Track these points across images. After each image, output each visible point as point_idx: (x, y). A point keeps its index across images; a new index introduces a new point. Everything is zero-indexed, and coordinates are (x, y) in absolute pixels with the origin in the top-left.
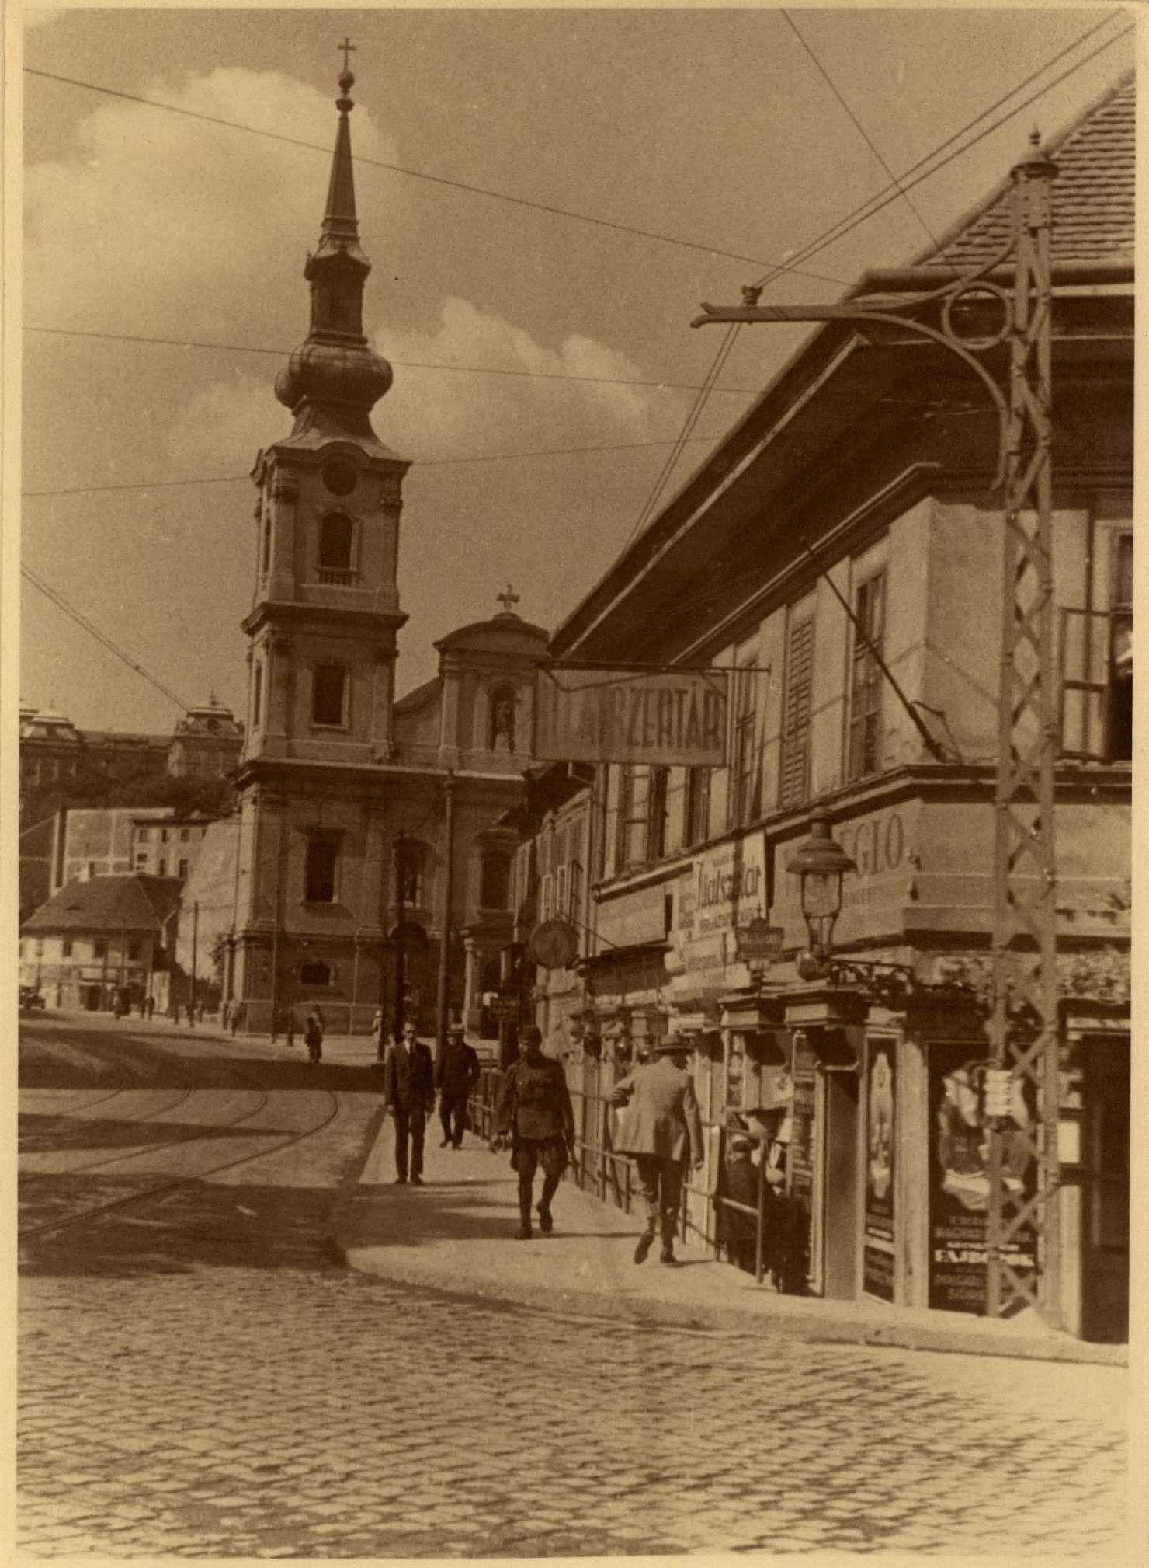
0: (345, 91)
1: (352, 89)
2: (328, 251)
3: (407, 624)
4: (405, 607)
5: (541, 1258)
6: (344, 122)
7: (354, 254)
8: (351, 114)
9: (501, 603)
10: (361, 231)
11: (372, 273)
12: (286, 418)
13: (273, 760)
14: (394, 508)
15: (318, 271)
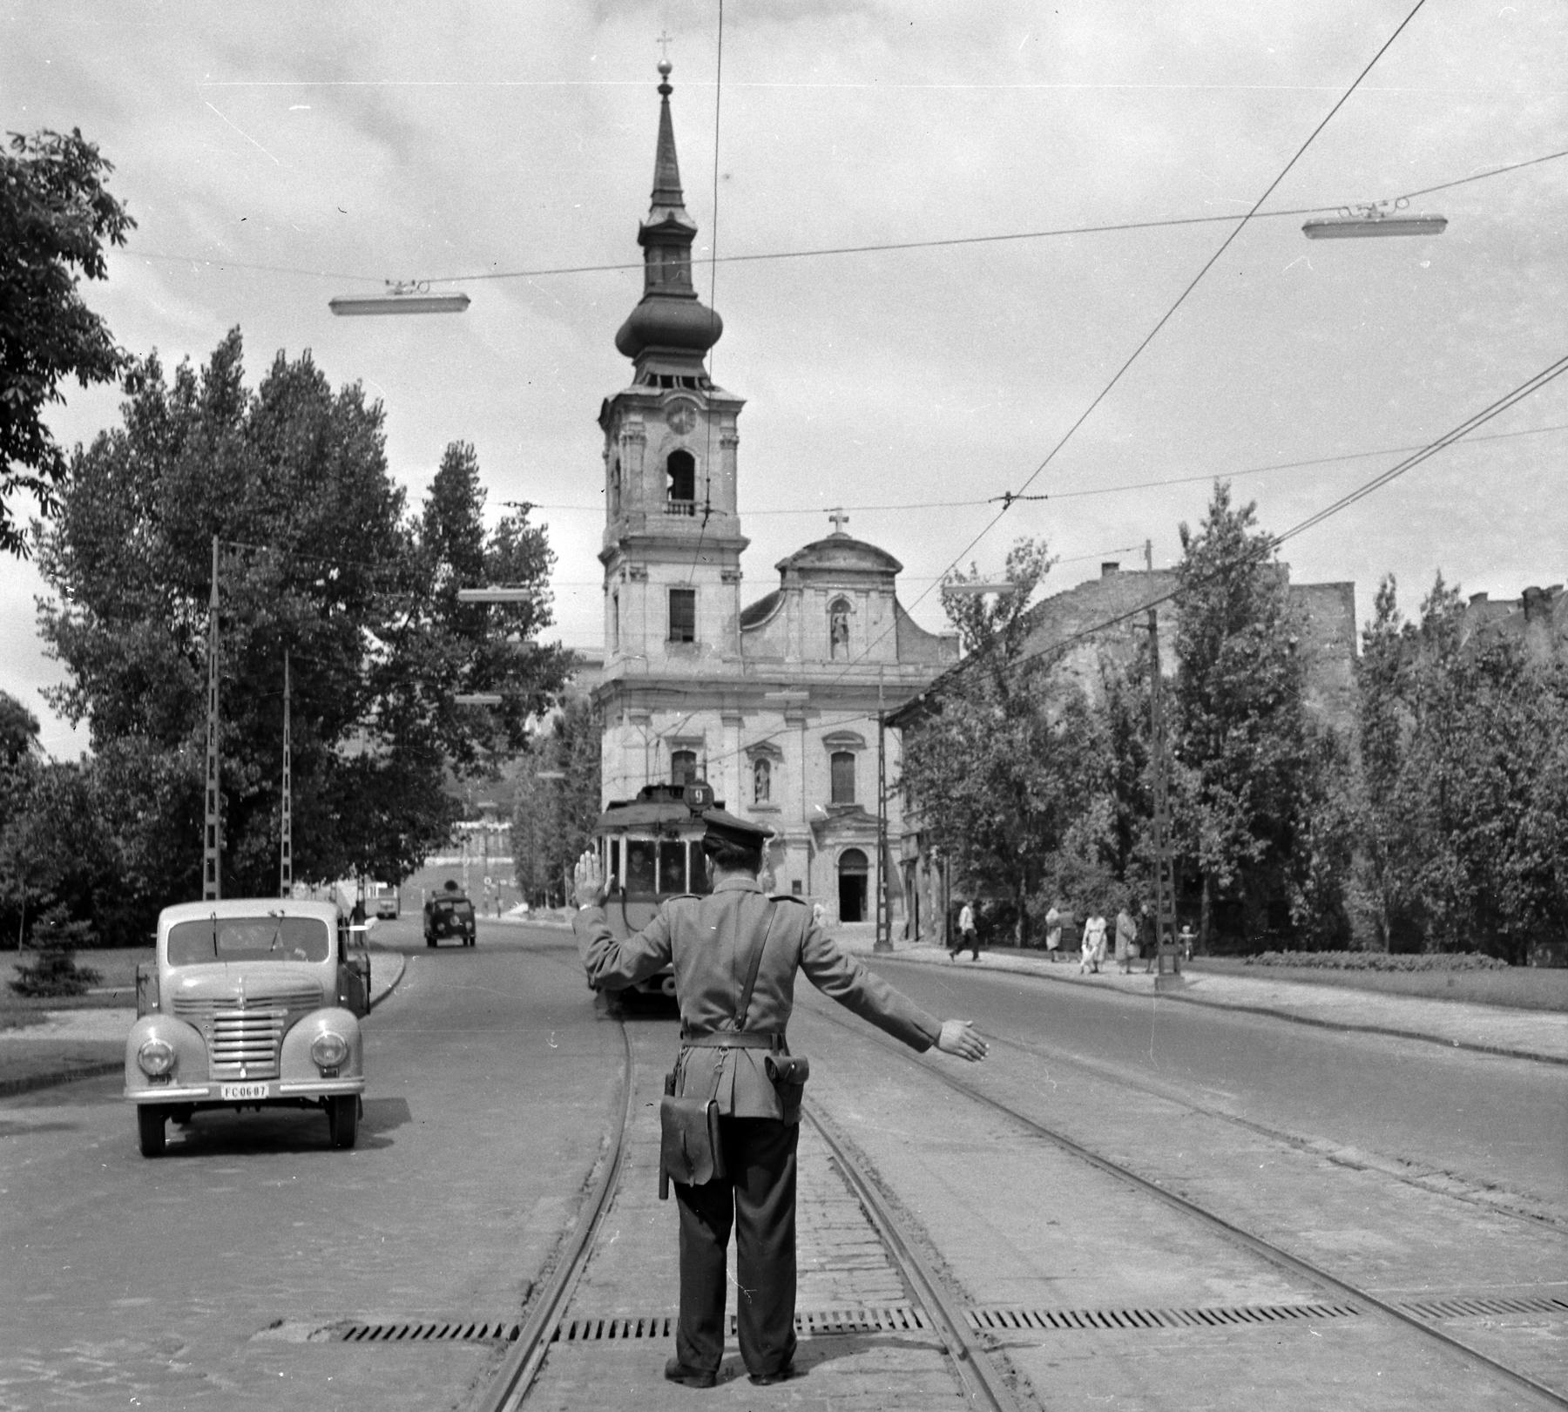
0: (665, 78)
1: (670, 76)
2: (659, 218)
3: (749, 547)
4: (744, 533)
5: (875, 1166)
6: (665, 103)
7: (682, 220)
8: (670, 97)
9: (833, 524)
10: (686, 198)
11: (698, 235)
12: (626, 367)
13: (263, 1091)
14: (731, 444)
15: (648, 237)
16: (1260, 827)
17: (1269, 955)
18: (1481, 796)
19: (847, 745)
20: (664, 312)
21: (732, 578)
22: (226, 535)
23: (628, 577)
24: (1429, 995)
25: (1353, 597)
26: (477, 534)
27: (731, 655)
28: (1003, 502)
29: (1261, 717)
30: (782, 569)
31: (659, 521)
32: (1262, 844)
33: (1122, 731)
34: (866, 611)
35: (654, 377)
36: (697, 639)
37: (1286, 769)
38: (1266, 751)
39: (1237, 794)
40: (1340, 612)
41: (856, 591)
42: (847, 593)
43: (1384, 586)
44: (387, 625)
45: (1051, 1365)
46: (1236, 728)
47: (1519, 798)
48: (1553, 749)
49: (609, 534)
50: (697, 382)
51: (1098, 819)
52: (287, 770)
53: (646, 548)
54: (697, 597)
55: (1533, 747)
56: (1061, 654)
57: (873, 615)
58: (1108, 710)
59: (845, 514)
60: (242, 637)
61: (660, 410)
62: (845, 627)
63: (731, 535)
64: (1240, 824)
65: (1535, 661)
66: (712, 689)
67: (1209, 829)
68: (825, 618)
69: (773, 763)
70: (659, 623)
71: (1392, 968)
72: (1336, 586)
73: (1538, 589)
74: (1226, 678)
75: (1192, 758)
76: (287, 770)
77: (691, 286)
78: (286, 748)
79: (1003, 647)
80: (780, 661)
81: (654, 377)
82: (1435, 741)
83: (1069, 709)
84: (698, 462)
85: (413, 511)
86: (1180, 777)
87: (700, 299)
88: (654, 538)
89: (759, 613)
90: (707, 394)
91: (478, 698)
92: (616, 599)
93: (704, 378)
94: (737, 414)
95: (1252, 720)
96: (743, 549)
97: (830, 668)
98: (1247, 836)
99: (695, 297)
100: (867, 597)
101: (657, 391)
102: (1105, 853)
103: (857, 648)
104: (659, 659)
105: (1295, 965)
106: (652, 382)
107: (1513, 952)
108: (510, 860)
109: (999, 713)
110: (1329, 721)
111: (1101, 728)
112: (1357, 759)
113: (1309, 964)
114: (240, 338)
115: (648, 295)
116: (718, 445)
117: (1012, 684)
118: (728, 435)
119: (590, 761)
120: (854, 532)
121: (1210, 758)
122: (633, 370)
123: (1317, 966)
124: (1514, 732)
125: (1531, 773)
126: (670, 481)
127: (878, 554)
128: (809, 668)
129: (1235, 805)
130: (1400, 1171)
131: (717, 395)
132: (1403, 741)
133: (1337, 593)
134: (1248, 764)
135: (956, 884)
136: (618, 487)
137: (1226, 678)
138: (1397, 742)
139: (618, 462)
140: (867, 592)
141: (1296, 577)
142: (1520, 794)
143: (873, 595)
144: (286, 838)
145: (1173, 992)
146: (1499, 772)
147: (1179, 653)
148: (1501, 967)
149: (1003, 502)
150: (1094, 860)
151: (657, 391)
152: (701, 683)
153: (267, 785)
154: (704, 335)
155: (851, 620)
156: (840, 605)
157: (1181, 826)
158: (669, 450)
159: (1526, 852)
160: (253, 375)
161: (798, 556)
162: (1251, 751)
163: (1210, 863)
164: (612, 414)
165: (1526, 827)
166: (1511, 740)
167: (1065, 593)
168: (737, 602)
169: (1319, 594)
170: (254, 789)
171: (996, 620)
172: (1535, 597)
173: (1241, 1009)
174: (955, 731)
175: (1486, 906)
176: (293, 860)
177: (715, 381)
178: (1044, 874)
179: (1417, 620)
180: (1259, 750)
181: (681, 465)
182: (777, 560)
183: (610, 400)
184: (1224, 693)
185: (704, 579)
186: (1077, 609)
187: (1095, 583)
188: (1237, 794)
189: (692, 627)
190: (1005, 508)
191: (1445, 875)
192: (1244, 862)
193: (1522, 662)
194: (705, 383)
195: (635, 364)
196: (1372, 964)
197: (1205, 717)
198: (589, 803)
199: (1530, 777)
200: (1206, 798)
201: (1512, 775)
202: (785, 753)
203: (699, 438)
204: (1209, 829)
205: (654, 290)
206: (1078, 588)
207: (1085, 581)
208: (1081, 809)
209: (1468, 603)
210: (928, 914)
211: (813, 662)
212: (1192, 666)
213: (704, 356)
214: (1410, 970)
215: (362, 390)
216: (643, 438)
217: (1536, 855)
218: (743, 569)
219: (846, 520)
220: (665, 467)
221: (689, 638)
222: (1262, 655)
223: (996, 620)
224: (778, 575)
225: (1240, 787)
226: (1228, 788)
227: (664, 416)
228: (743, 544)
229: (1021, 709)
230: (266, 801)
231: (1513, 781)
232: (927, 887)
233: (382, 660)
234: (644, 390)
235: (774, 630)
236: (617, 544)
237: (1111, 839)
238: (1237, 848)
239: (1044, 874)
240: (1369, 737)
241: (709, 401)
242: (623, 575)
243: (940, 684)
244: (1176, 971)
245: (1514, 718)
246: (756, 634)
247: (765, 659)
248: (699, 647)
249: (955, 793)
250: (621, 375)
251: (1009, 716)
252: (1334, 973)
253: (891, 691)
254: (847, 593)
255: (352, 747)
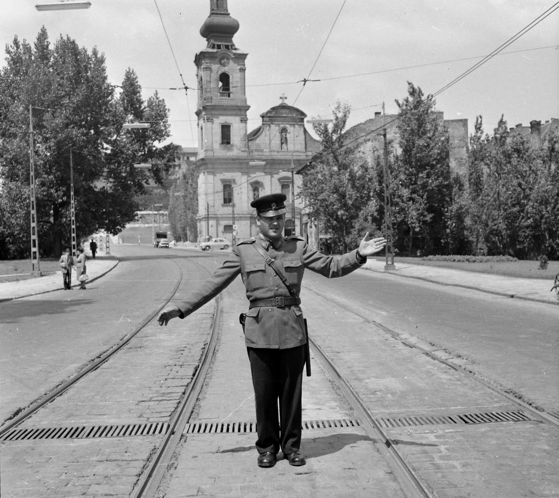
3: (250, 109)
4: (249, 103)
12: (204, 41)
14: (243, 70)
16: (430, 210)
17: (431, 257)
18: (512, 198)
19: (287, 182)
20: (219, 20)
21: (244, 120)
22: (46, 106)
23: (206, 120)
24: (483, 272)
25: (467, 125)
26: (140, 102)
27: (245, 149)
28: (303, 83)
29: (431, 169)
30: (263, 117)
31: (218, 99)
32: (431, 215)
33: (380, 175)
34: (294, 132)
35: (214, 45)
36: (231, 143)
37: (440, 188)
38: (433, 182)
39: (422, 197)
40: (462, 129)
41: (290, 125)
42: (286, 126)
43: (477, 120)
44: (109, 138)
45: (196, 457)
46: (422, 173)
47: (526, 199)
48: (539, 180)
49: (199, 104)
50: (230, 47)
51: (371, 207)
52: (72, 193)
53: (212, 109)
54: (231, 128)
55: (531, 180)
56: (358, 146)
57: (296, 134)
58: (375, 167)
59: (285, 96)
60: (53, 144)
61: (216, 57)
62: (286, 138)
63: (244, 104)
64: (424, 209)
65: (533, 148)
66: (237, 161)
67: (412, 210)
68: (278, 135)
69: (260, 189)
70: (218, 138)
71: (474, 261)
72: (461, 120)
73: (536, 121)
74: (418, 155)
75: (406, 185)
76: (72, 193)
77: (227, 10)
78: (72, 185)
79: (337, 145)
80: (262, 151)
81: (214, 45)
82: (496, 178)
83: (362, 166)
84: (231, 77)
85: (118, 94)
86: (401, 191)
87: (231, 15)
88: (215, 106)
89: (256, 133)
90: (234, 51)
91: (143, 165)
92: (202, 128)
93: (233, 45)
94: (245, 59)
95: (427, 171)
96: (248, 109)
97: (280, 153)
98: (426, 213)
99: (229, 14)
100: (294, 127)
101: (215, 50)
102: (374, 220)
103: (291, 147)
104: (220, 152)
105: (440, 261)
106: (213, 47)
107: (521, 255)
108: (168, 225)
109: (335, 168)
110: (457, 171)
111: (373, 173)
112: (467, 185)
113: (445, 260)
114: (46, 30)
115: (212, 14)
116: (238, 71)
117: (340, 158)
118: (242, 67)
119: (194, 189)
120: (289, 102)
121: (412, 185)
122: (207, 43)
123: (447, 261)
124: (524, 174)
125: (531, 189)
126: (221, 84)
127: (297, 110)
128: (272, 153)
129: (422, 202)
130: (427, 348)
131: (238, 52)
132: (485, 178)
133: (461, 123)
134: (427, 186)
135: (321, 232)
136: (202, 87)
137: (418, 155)
138: (481, 179)
139: (201, 77)
140: (294, 125)
141: (446, 117)
142: (527, 197)
143: (296, 126)
144: (73, 218)
145: (391, 271)
146: (519, 189)
147: (401, 147)
148: (515, 261)
149: (303, 83)
150: (370, 222)
151: (215, 50)
152: (233, 159)
153: (65, 198)
154: (233, 29)
155: (288, 136)
156: (284, 130)
157: (402, 210)
158: (220, 72)
159: (529, 218)
160: (52, 43)
161: (268, 112)
162: (428, 181)
163: (412, 223)
164: (199, 59)
165: (528, 209)
166: (523, 177)
167: (361, 124)
168: (246, 131)
169: (454, 123)
170: (60, 201)
171: (333, 134)
172: (535, 124)
173: (412, 277)
174: (319, 175)
175: (514, 238)
176: (76, 227)
177: (237, 46)
178: (353, 227)
179: (491, 134)
180: (430, 181)
181: (225, 78)
182: (261, 113)
183: (198, 54)
184: (417, 161)
185: (234, 121)
186: (365, 129)
187: (372, 120)
188: (422, 197)
189: (230, 139)
190: (304, 85)
191: (498, 227)
192: (425, 222)
193: (528, 148)
194: (233, 47)
195: (207, 40)
196: (467, 260)
197: (411, 170)
198: (195, 204)
199: (530, 191)
200: (411, 199)
201: (524, 190)
202: (264, 184)
203: (231, 68)
204: (412, 210)
205: (214, 12)
206: (366, 122)
207: (368, 119)
208: (365, 204)
209: (515, 127)
210: (312, 243)
211: (274, 151)
212: (407, 151)
213: (232, 37)
214: (481, 262)
215: (97, 50)
216: (210, 68)
217: (531, 219)
218: (248, 117)
219: (286, 98)
220: (219, 79)
221: (229, 143)
222: (431, 146)
223: (333, 134)
224: (261, 119)
225: (423, 195)
226: (419, 195)
227: (218, 60)
228: (248, 108)
229: (343, 167)
230: (66, 204)
231: (524, 193)
232: (311, 233)
233: (109, 152)
234: (210, 50)
235: (261, 140)
236: (201, 108)
237: (376, 214)
238: (422, 217)
239: (353, 227)
240: (472, 177)
241: (235, 54)
242: (204, 119)
243: (315, 158)
244: (393, 264)
245: (524, 169)
246: (253, 142)
247: (257, 150)
248: (232, 146)
249: (319, 198)
250: (202, 45)
251: (339, 170)
252: (454, 263)
253: (298, 161)
254: (286, 126)
255: (100, 184)
